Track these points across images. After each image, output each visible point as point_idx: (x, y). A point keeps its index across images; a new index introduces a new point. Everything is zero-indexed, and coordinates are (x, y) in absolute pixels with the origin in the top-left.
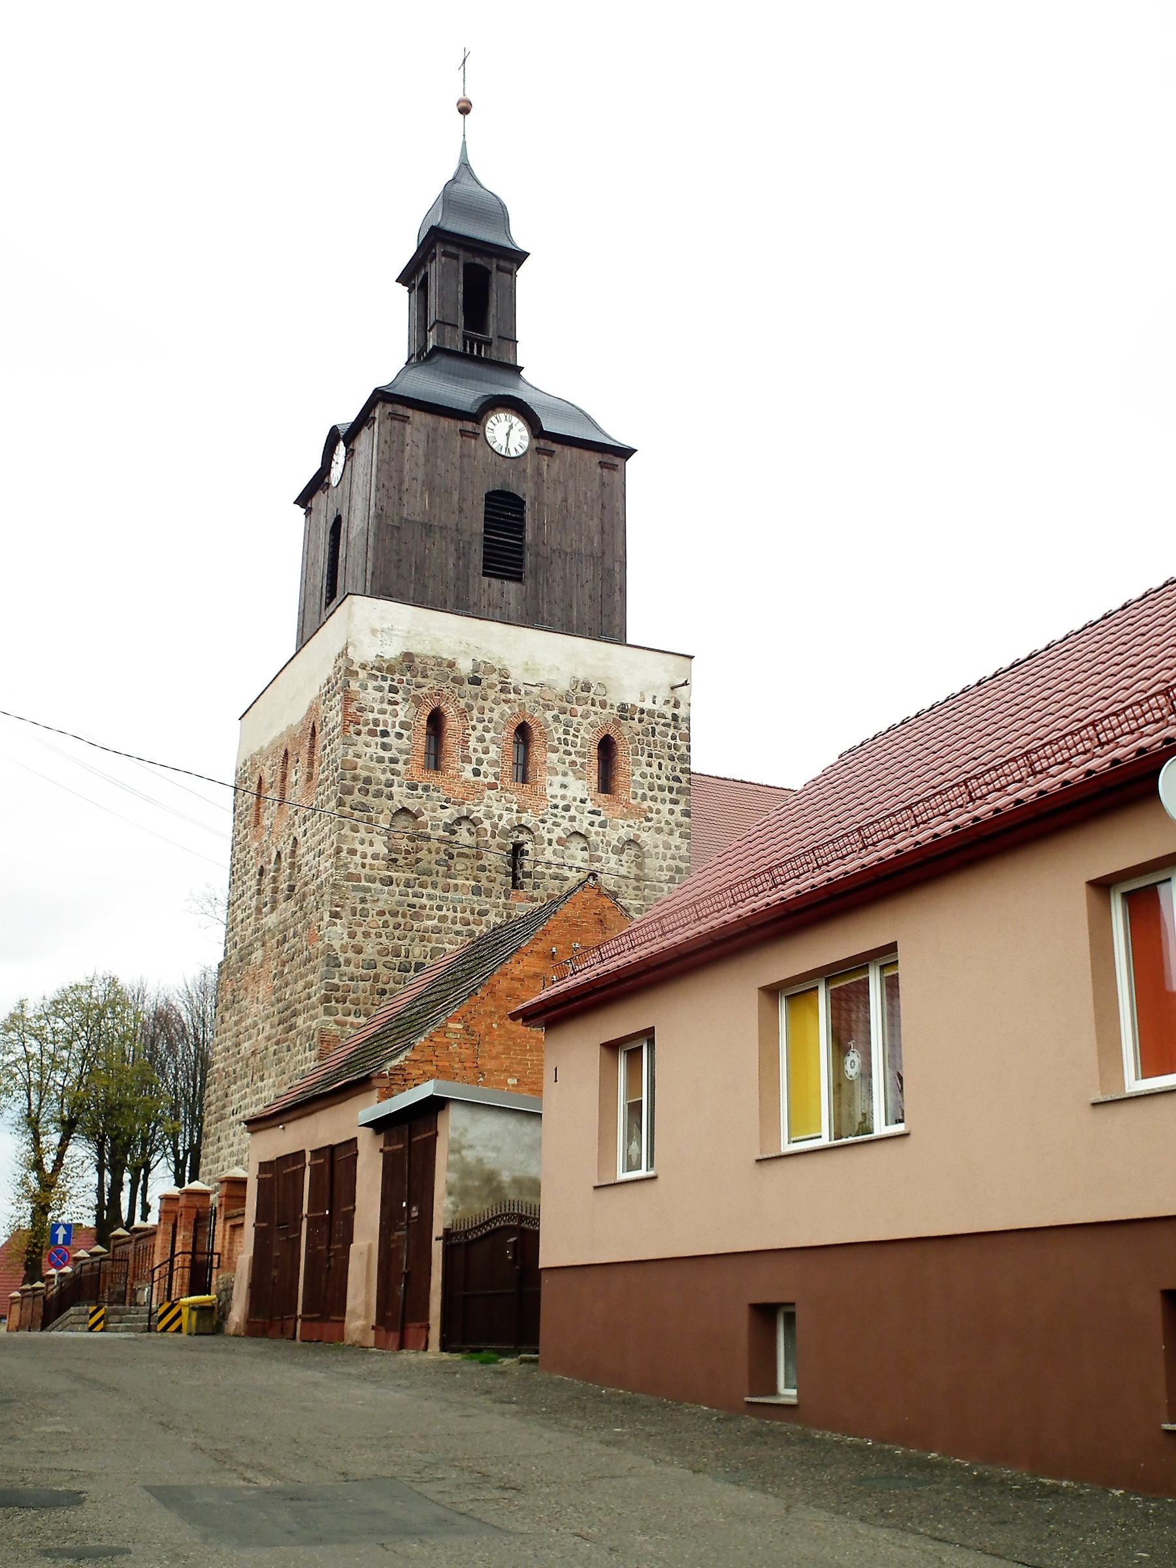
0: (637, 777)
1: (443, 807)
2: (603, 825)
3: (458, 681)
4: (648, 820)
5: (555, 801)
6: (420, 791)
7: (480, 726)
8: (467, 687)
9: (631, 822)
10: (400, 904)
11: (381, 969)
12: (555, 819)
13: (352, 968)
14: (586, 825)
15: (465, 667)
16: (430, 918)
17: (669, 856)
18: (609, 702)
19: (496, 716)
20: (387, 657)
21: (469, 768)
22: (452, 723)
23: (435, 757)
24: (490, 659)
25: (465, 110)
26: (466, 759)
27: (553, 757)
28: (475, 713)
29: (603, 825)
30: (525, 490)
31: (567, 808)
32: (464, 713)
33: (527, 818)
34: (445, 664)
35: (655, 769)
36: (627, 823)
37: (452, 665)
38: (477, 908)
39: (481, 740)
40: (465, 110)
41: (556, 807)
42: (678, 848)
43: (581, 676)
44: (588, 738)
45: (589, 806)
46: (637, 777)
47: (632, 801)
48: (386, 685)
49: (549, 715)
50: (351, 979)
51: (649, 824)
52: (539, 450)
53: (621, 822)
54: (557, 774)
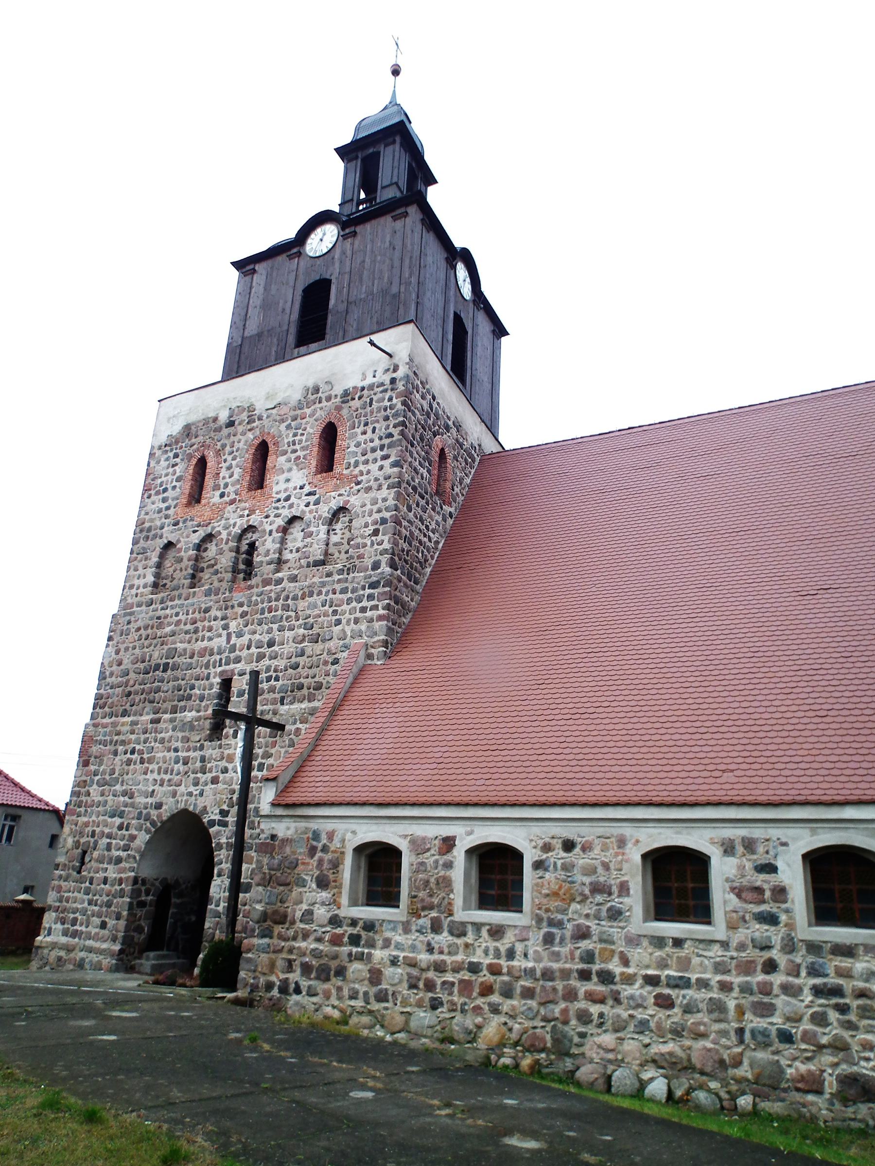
0: (352, 449)
1: (194, 532)
2: (317, 503)
3: (218, 430)
4: (358, 483)
5: (278, 496)
6: (181, 524)
7: (229, 458)
8: (225, 431)
9: (342, 491)
10: (151, 619)
11: (132, 675)
12: (276, 511)
13: (113, 679)
14: (302, 507)
15: (223, 417)
16: (169, 624)
17: (375, 511)
18: (333, 394)
19: (241, 445)
20: (174, 434)
21: (218, 493)
22: (211, 463)
23: (196, 497)
24: (242, 402)
25: (396, 72)
26: (216, 487)
27: (282, 459)
28: (228, 449)
29: (317, 503)
30: (334, 273)
31: (287, 499)
32: (218, 453)
33: (255, 520)
34: (211, 420)
35: (369, 434)
36: (338, 493)
37: (215, 419)
38: (203, 606)
39: (229, 468)
40: (396, 72)
41: (279, 500)
42: (385, 500)
43: (310, 384)
44: (313, 430)
45: (307, 489)
46: (352, 449)
47: (345, 472)
48: (171, 454)
49: (283, 427)
50: (111, 688)
51: (359, 487)
52: (345, 237)
53: (333, 494)
54: (283, 472)
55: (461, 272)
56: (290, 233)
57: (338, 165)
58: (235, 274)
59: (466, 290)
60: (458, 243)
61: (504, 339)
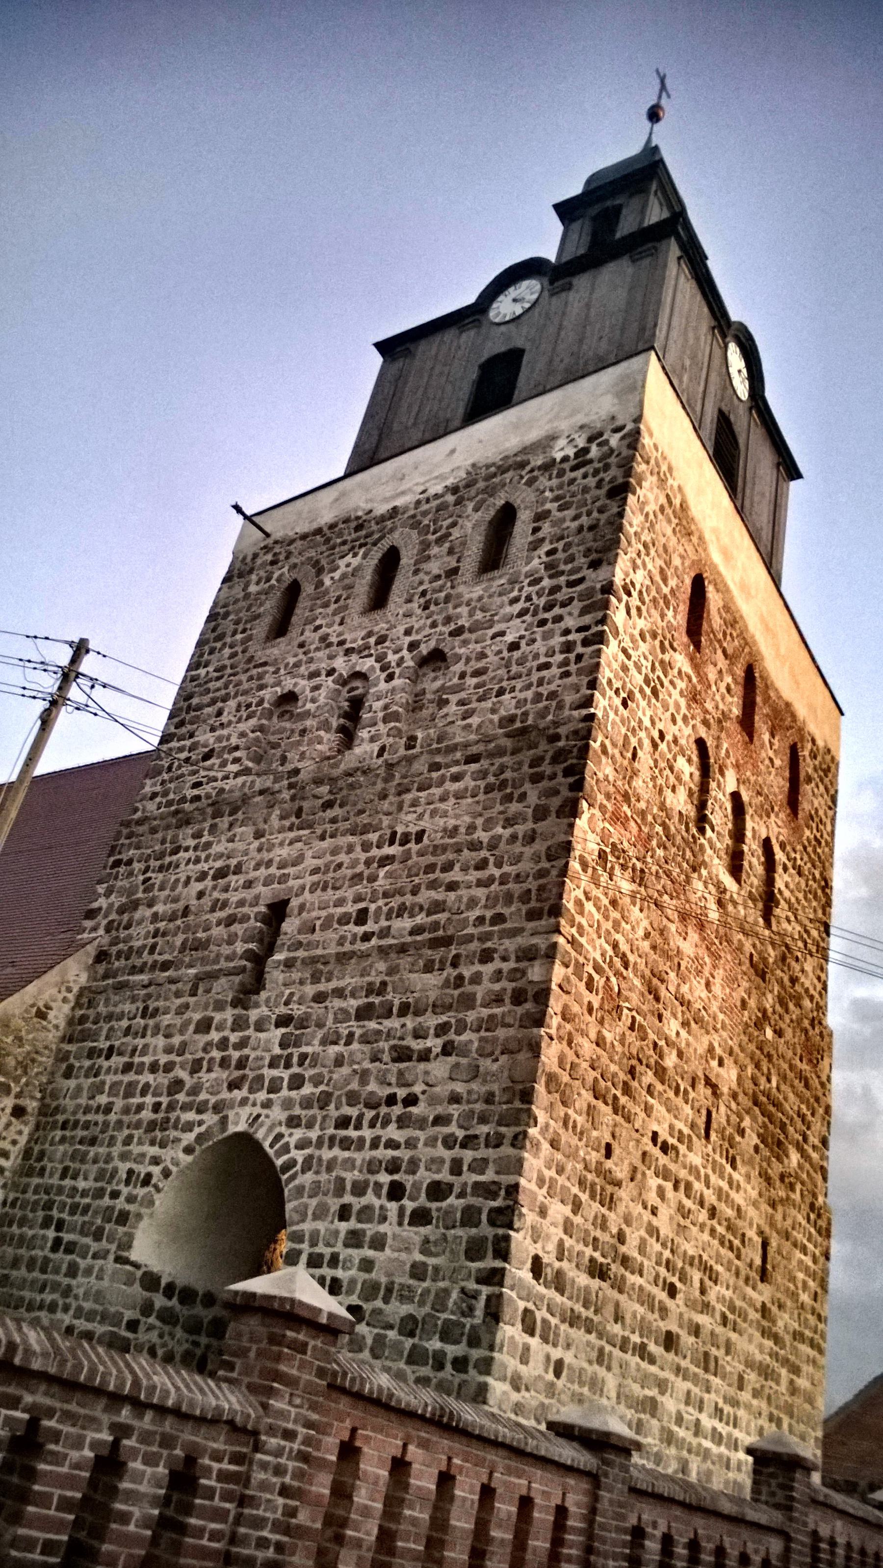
40: (654, 115)
55: (736, 361)
56: (470, 298)
57: (557, 228)
58: (377, 360)
59: (742, 389)
60: (735, 315)
61: (794, 485)
